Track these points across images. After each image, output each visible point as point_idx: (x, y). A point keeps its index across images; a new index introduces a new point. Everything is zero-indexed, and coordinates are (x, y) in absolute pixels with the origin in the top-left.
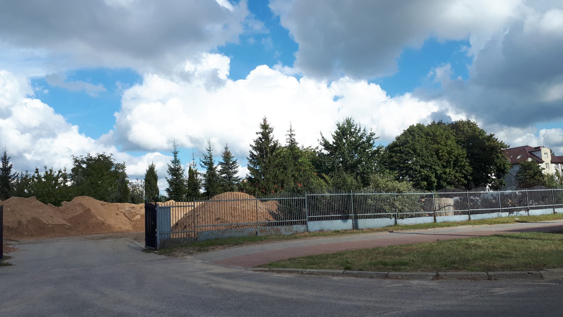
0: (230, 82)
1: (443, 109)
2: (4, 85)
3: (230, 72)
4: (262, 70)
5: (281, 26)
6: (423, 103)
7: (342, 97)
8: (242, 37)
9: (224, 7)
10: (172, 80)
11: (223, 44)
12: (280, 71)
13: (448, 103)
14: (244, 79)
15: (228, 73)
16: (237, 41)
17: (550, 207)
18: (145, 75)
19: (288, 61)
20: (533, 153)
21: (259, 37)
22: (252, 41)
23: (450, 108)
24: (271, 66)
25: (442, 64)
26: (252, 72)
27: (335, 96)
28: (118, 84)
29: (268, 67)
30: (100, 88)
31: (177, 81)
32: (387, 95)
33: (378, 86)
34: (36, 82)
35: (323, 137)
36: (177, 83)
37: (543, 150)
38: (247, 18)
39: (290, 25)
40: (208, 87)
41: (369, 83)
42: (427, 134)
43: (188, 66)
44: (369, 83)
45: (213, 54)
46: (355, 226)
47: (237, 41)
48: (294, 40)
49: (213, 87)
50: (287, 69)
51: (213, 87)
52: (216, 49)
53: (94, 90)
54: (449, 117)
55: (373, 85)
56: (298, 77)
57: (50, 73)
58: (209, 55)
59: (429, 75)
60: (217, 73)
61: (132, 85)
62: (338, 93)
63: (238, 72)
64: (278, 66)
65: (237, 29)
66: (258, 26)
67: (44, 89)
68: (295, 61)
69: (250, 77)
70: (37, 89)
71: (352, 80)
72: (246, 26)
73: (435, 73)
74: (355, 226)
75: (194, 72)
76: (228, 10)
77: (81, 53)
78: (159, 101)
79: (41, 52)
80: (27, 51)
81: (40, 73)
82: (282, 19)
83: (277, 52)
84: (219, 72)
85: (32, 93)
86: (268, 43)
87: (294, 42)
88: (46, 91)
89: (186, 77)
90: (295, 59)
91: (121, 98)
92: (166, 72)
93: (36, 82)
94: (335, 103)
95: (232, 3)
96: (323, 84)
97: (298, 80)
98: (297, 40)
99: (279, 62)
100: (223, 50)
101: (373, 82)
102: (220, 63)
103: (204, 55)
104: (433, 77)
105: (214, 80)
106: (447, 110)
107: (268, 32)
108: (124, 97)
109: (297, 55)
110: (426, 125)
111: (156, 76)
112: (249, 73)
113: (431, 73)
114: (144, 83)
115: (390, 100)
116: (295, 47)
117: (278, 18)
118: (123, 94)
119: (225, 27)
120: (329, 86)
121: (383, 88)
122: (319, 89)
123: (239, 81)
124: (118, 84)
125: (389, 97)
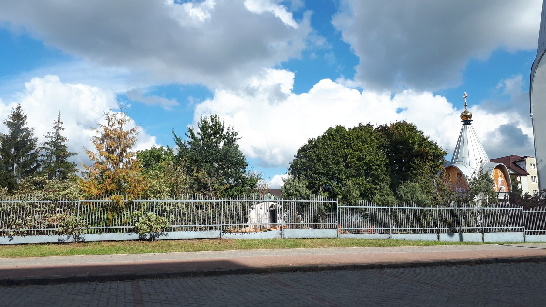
0: (294, 95)
1: (513, 121)
2: (94, 100)
3: (294, 86)
4: (326, 83)
5: (342, 41)
6: (491, 116)
7: (406, 109)
8: (305, 53)
9: (288, 25)
10: (238, 95)
11: (286, 60)
12: (342, 84)
13: (519, 116)
14: (307, 93)
15: (292, 88)
16: (299, 57)
17: (432, 232)
18: (217, 91)
19: (350, 75)
20: (518, 164)
21: (321, 52)
22: (313, 56)
23: (521, 121)
24: (333, 80)
25: (513, 76)
26: (315, 86)
27: (398, 109)
28: (190, 98)
29: (331, 81)
30: (174, 102)
31: (243, 96)
32: (453, 108)
33: (444, 98)
34: (120, 98)
35: (176, 137)
36: (243, 97)
37: (529, 161)
38: (310, 34)
39: (351, 39)
40: (271, 101)
41: (434, 95)
42: (343, 137)
43: (254, 82)
44: (434, 95)
45: (279, 70)
46: (461, 239)
47: (299, 57)
48: (355, 54)
49: (276, 101)
50: (349, 82)
51: (276, 101)
52: (280, 65)
53: (168, 104)
54: (520, 130)
55: (438, 97)
56: (361, 91)
57: (130, 89)
58: (274, 71)
59: (497, 87)
60: (280, 88)
61: (203, 100)
62: (402, 106)
63: (302, 86)
64: (341, 80)
65: (300, 45)
66: (320, 42)
67: (127, 103)
68: (356, 75)
69: (312, 91)
70: (122, 103)
71: (414, 93)
72: (309, 42)
73: (505, 84)
74: (461, 239)
75: (258, 88)
76: (292, 28)
77: (160, 70)
78: (228, 114)
79: (124, 70)
80: (113, 69)
81: (123, 89)
82: (343, 35)
83: (339, 67)
84: (281, 86)
85: (117, 107)
86: (331, 58)
87: (355, 56)
88: (129, 106)
89: (251, 92)
90: (355, 72)
91: (194, 111)
92: (233, 88)
93: (120, 98)
94: (398, 115)
95: (296, 21)
96: (385, 97)
97: (361, 93)
98: (358, 54)
99: (342, 76)
100: (286, 66)
101: (439, 94)
102: (286, 79)
103: (269, 71)
104: (502, 89)
105: (277, 95)
106: (518, 123)
107: (331, 47)
108: (196, 111)
109: (358, 68)
110: (347, 129)
111: (223, 91)
112: (313, 87)
113: (500, 85)
114: (214, 99)
115: (456, 112)
116: (356, 60)
117: (340, 33)
118: (195, 108)
119: (290, 43)
120: (392, 97)
121: (449, 100)
122: (380, 101)
123: (302, 94)
124: (190, 98)
125: (456, 109)
